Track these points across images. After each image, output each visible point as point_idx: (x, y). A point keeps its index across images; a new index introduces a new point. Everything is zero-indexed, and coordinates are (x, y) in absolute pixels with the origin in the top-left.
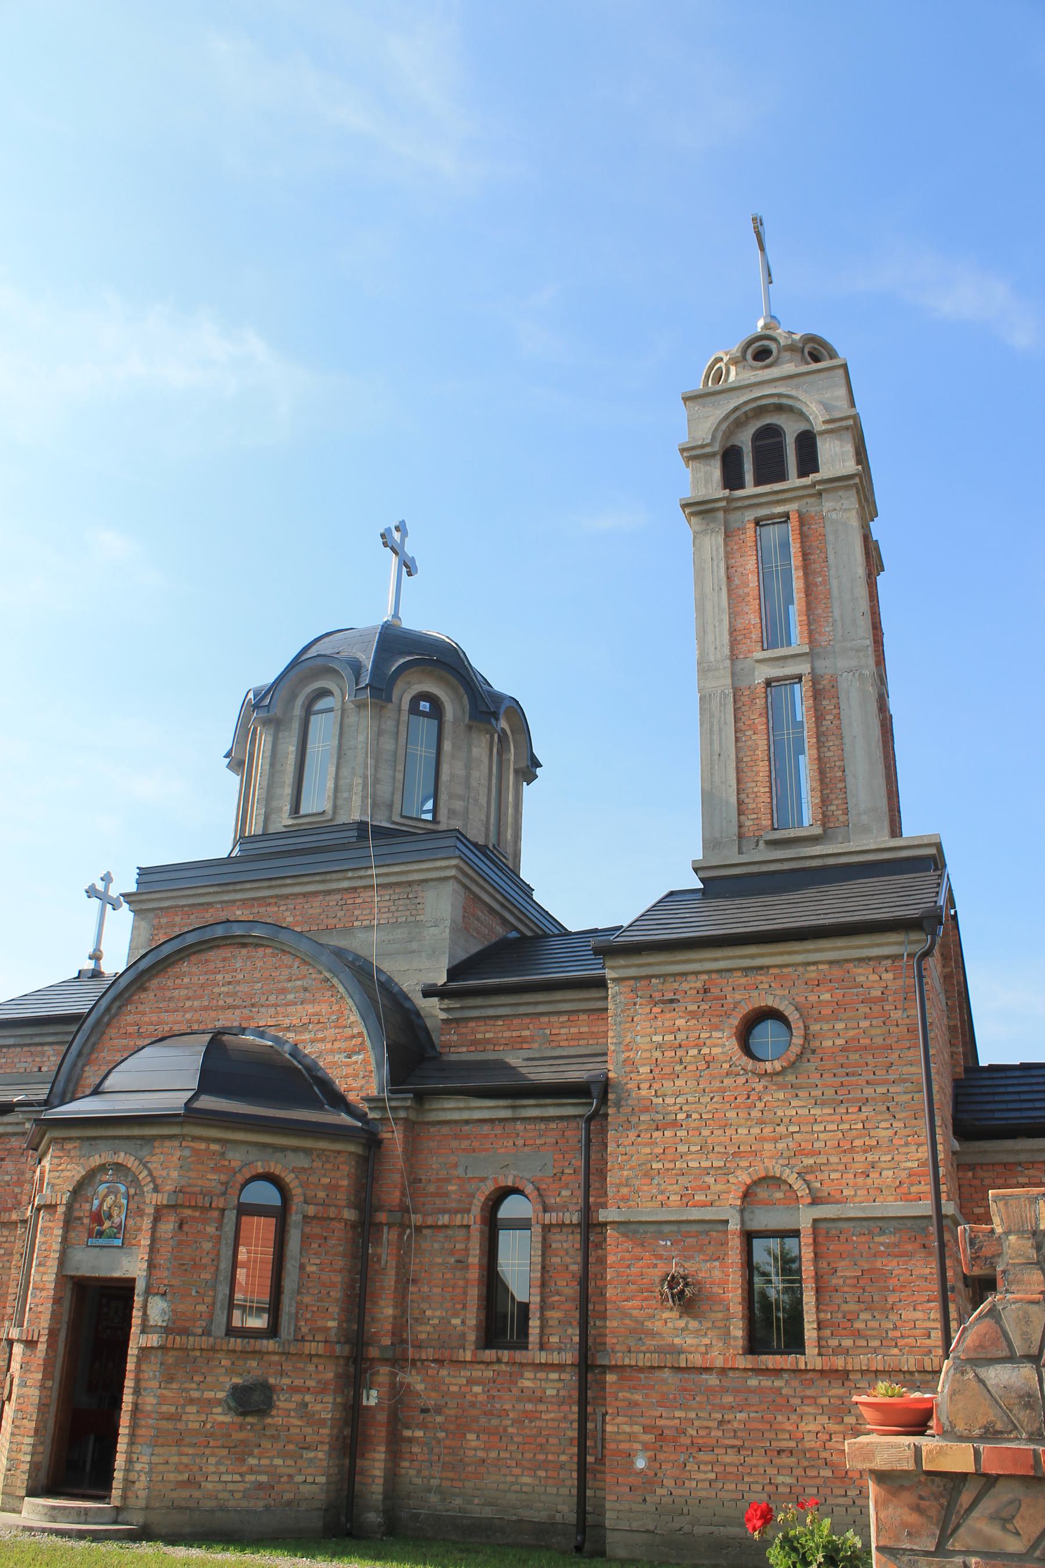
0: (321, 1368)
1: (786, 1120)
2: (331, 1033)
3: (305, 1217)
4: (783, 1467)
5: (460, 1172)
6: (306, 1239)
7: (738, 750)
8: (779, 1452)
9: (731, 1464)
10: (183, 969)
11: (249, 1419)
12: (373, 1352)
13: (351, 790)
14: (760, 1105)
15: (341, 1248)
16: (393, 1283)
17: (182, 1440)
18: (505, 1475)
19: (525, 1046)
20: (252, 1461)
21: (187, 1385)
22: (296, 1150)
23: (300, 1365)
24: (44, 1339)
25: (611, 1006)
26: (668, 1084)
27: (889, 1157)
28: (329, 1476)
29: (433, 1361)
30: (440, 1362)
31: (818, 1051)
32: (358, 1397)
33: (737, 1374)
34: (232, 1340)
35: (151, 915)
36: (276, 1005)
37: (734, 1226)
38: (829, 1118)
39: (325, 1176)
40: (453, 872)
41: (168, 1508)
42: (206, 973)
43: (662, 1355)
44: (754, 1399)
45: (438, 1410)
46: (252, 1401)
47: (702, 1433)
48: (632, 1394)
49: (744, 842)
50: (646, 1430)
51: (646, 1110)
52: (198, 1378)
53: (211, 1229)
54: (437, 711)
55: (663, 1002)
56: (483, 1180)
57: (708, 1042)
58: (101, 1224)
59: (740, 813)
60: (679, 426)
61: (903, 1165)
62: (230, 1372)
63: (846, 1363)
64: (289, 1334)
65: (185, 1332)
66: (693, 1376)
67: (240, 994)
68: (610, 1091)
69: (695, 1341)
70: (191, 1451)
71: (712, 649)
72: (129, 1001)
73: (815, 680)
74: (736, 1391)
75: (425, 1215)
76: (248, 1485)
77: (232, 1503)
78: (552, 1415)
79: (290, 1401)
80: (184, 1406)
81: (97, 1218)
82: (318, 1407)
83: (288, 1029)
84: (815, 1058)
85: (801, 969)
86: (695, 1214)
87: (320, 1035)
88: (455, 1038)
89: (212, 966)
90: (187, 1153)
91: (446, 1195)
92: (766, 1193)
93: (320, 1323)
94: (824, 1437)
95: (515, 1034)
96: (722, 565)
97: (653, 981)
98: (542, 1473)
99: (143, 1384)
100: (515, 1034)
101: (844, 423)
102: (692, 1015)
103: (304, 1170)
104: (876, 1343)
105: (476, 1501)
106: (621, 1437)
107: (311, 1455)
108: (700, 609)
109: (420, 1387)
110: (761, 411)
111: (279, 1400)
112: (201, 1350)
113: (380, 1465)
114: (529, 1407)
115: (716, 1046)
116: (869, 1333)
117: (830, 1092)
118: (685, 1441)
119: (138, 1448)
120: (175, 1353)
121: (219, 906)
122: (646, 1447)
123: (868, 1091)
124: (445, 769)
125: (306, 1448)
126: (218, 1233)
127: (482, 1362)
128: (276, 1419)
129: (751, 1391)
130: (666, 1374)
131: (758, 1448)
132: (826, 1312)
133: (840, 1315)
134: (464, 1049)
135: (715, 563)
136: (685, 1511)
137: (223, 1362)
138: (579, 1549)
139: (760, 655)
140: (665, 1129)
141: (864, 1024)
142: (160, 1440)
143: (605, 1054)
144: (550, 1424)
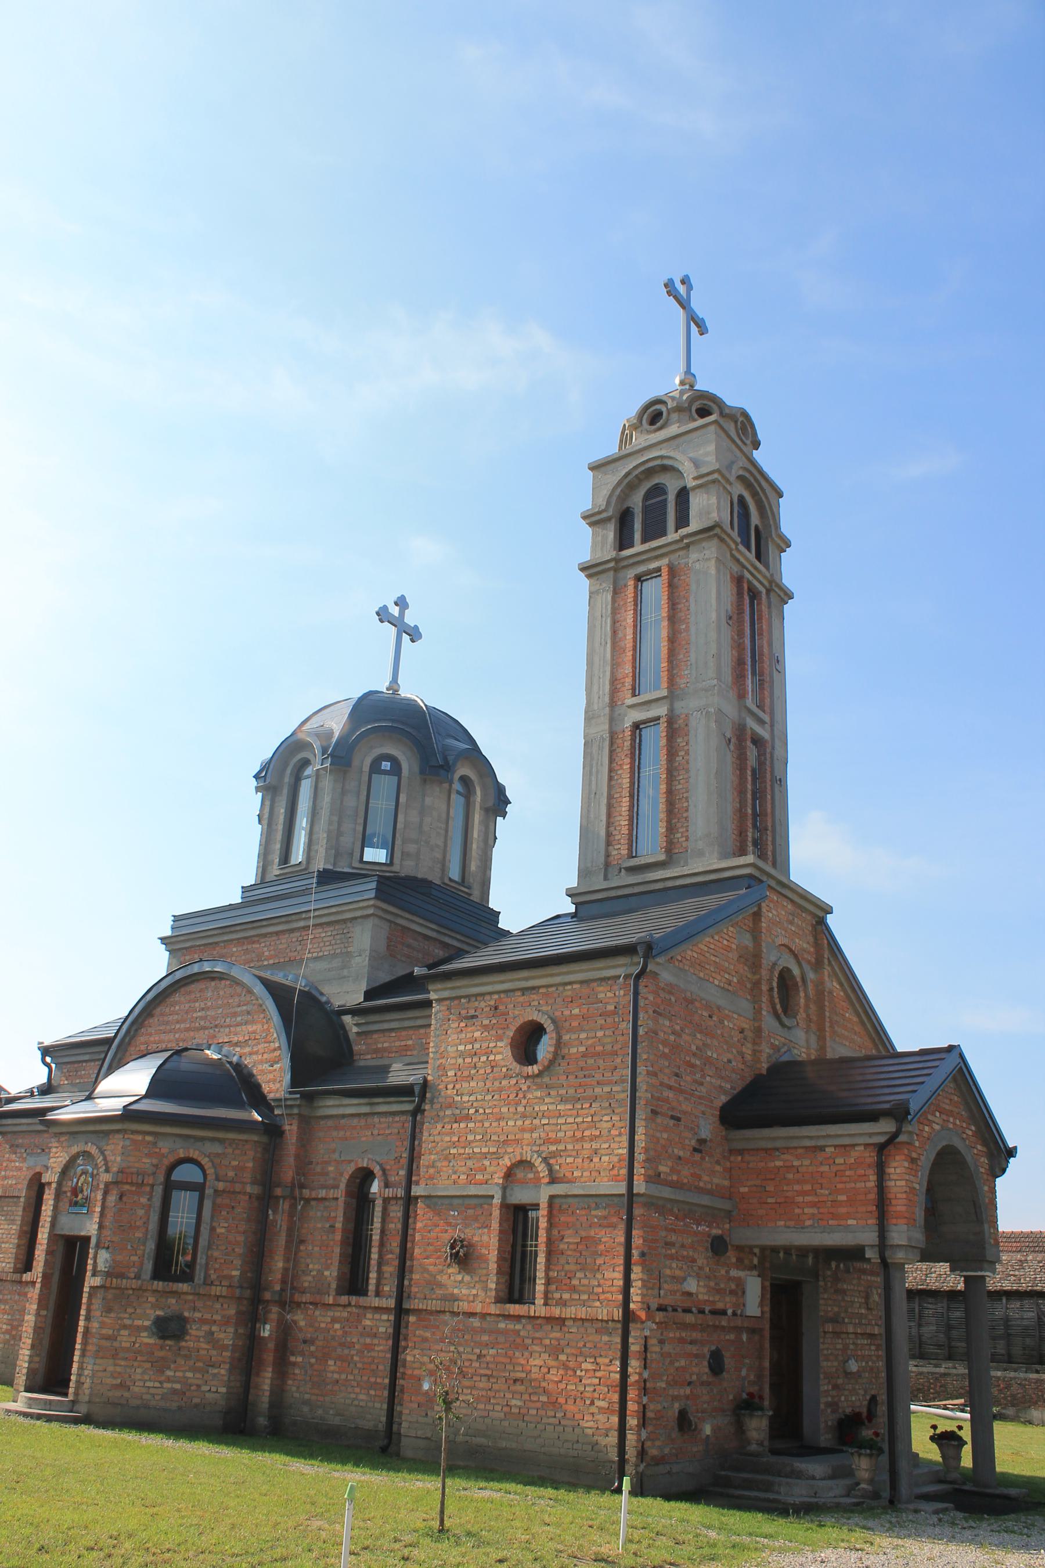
0: (225, 1306)
1: (540, 1114)
2: (261, 1047)
3: (216, 1191)
5: (336, 1156)
6: (216, 1209)
7: (610, 787)
8: (515, 1381)
11: (168, 1342)
14: (524, 1102)
19: (409, 1053)
21: (122, 1315)
22: (213, 1140)
23: (210, 1303)
24: (39, 1280)
25: (433, 1022)
26: (465, 1085)
27: (606, 1146)
28: (228, 1388)
29: (311, 1303)
32: (253, 1329)
33: (493, 1319)
35: (180, 953)
36: (229, 1026)
37: (497, 1201)
38: (569, 1113)
39: (234, 1159)
40: (371, 911)
42: (189, 1001)
44: (501, 1339)
46: (171, 1329)
47: (467, 1364)
49: (610, 869)
51: (450, 1106)
52: (130, 1310)
53: (144, 1200)
54: (396, 768)
55: (467, 1018)
56: (350, 1162)
58: (77, 1197)
59: (608, 843)
60: (583, 493)
61: (616, 1152)
62: (154, 1307)
64: (199, 1279)
65: (121, 1276)
69: (464, 1291)
70: (123, 1363)
71: (596, 700)
72: (142, 1025)
73: (671, 721)
74: (491, 1332)
75: (312, 1189)
77: (153, 1403)
78: (381, 1348)
80: (119, 1330)
82: (222, 1336)
83: (236, 1044)
84: (564, 1063)
85: (561, 988)
86: (473, 1190)
87: (255, 1049)
89: (193, 996)
90: (128, 1143)
93: (225, 1272)
94: (544, 1370)
96: (609, 621)
97: (463, 1000)
98: (372, 1392)
99: (92, 1314)
100: (403, 1043)
101: (710, 478)
102: (486, 1028)
103: (218, 1155)
104: (585, 1297)
105: (331, 1412)
106: (416, 1365)
107: (216, 1371)
108: (590, 663)
109: (302, 1323)
110: (650, 472)
112: (133, 1289)
113: (268, 1381)
114: (368, 1340)
115: (499, 1053)
116: (581, 1288)
117: (571, 1091)
119: (86, 1360)
120: (113, 1291)
123: (598, 1090)
124: (401, 818)
125: (212, 1366)
127: (339, 1305)
129: (499, 1332)
130: (447, 1317)
133: (563, 1274)
134: (369, 1057)
138: (384, 1450)
139: (630, 701)
141: (600, 1034)
142: (101, 1354)
143: (427, 1062)
144: (381, 1354)
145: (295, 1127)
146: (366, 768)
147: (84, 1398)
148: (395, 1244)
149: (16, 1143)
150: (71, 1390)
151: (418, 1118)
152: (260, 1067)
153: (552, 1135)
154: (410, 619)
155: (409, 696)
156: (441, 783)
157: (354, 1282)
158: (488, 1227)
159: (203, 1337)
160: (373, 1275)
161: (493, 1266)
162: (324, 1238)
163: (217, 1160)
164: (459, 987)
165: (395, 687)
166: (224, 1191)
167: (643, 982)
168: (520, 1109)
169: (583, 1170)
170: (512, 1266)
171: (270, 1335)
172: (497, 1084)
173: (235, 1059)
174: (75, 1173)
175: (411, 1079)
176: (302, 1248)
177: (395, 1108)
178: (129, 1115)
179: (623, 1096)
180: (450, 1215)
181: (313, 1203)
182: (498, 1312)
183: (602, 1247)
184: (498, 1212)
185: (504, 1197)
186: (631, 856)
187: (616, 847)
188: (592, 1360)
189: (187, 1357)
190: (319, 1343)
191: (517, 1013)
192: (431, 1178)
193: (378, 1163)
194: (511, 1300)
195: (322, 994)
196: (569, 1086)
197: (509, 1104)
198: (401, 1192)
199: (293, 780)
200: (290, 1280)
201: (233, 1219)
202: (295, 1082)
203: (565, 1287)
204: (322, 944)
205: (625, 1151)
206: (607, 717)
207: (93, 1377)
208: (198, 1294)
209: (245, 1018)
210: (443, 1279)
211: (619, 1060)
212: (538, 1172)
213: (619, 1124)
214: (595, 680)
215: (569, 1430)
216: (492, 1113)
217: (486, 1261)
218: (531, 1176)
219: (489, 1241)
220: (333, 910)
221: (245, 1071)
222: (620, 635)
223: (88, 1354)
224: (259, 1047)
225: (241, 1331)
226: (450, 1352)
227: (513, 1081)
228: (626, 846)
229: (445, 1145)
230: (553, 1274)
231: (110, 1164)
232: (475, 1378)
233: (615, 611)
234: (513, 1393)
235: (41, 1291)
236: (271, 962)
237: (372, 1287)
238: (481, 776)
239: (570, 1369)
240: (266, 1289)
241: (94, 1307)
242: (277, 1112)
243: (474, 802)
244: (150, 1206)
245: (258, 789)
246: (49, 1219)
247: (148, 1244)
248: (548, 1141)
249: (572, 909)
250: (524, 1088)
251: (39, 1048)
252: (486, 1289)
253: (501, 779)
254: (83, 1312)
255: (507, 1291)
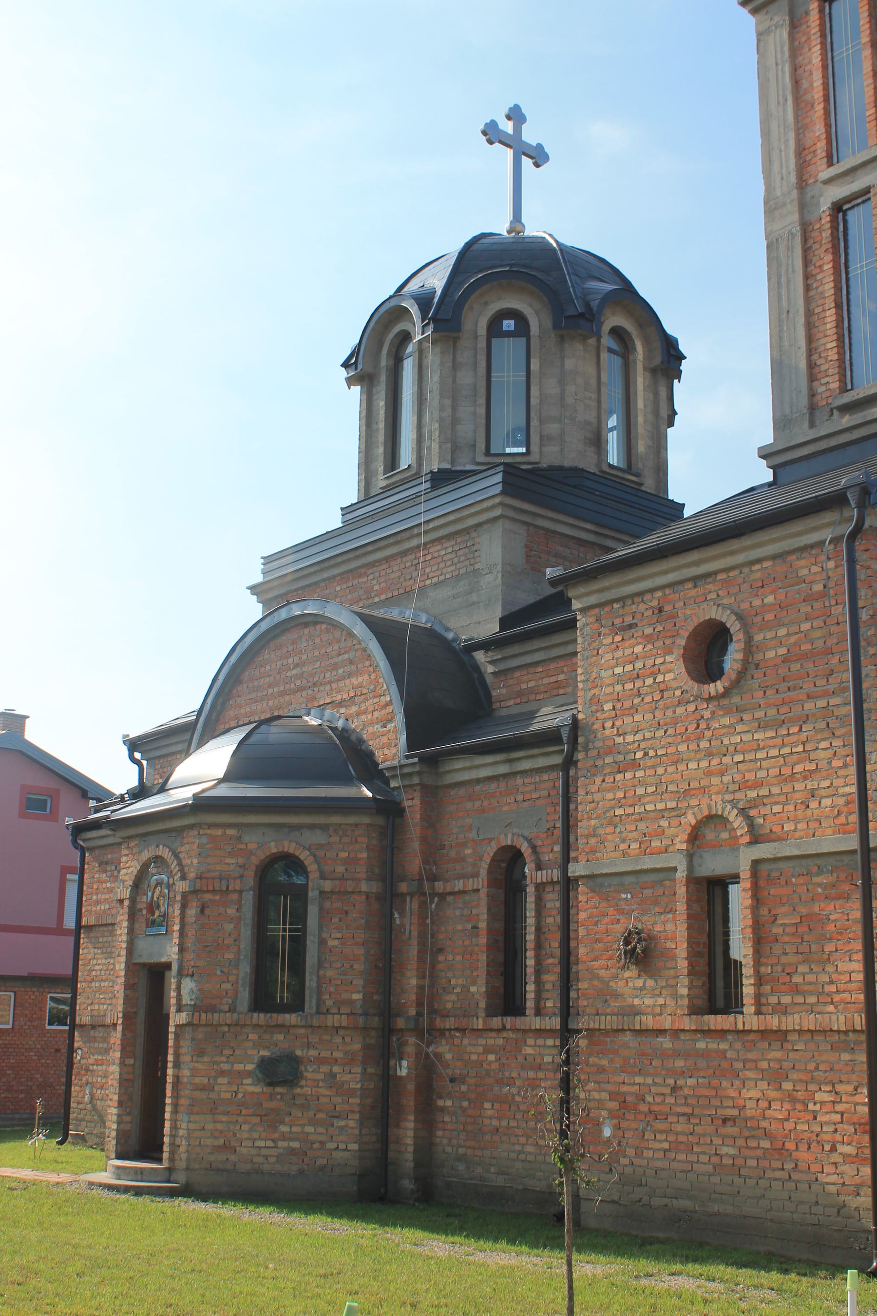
0: (348, 1039)
4: (727, 1136)
5: (473, 835)
7: (808, 300)
8: (724, 1121)
9: (682, 1133)
10: (266, 657)
11: (279, 1090)
12: (400, 1023)
13: (430, 438)
14: (708, 734)
15: (363, 921)
16: (416, 953)
17: (216, 1108)
18: (514, 1144)
19: (561, 691)
20: (284, 1129)
22: (312, 827)
24: (120, 1022)
26: (628, 720)
27: (826, 784)
29: (457, 1029)
30: (463, 1031)
31: (762, 665)
32: (386, 1067)
33: (688, 1036)
34: (255, 1015)
38: (771, 742)
39: (343, 850)
40: (498, 512)
41: (206, 1169)
43: (620, 1017)
44: (702, 1063)
45: (462, 1080)
46: (280, 1072)
47: (658, 1099)
48: (600, 1059)
50: (613, 1096)
51: (609, 752)
52: (227, 1052)
53: (231, 911)
54: (523, 328)
57: (662, 668)
58: (153, 915)
61: (841, 791)
63: (780, 1022)
64: (311, 1008)
65: (212, 1009)
66: (649, 1039)
67: (305, 675)
68: (579, 734)
69: (648, 1001)
70: (224, 1118)
71: (778, 184)
74: (686, 1056)
76: (281, 1151)
77: (266, 1167)
79: (319, 1072)
80: (215, 1078)
81: (152, 907)
82: (347, 1077)
83: (341, 704)
84: (758, 674)
85: (746, 570)
86: (648, 863)
87: (363, 707)
88: (504, 691)
89: (285, 650)
90: (204, 840)
91: (463, 859)
92: (713, 834)
93: (345, 996)
94: (763, 1104)
95: (552, 679)
96: (787, 68)
97: (615, 606)
99: (182, 1058)
100: (552, 679)
102: (649, 639)
103: (321, 846)
104: (812, 999)
105: (493, 1170)
107: (342, 1123)
108: (766, 134)
109: (448, 1056)
111: (307, 1071)
112: (229, 1025)
113: (410, 1133)
114: (531, 1074)
115: (669, 671)
116: (807, 987)
117: (772, 712)
118: (644, 1108)
119: (180, 1116)
121: (323, 584)
122: (612, 1115)
123: (809, 706)
126: (238, 914)
127: (492, 1030)
128: (305, 1089)
130: (628, 1037)
131: (705, 1115)
132: (765, 964)
133: (779, 969)
134: (511, 702)
135: (780, 67)
136: (644, 1182)
137: (251, 1036)
139: (825, 174)
140: (626, 771)
141: (805, 626)
145: (417, 802)
146: (482, 331)
147: (181, 1164)
148: (554, 944)
149: (105, 859)
150: (165, 1155)
151: (572, 773)
152: (370, 730)
153: (750, 776)
154: (530, 135)
155: (535, 234)
156: (585, 338)
157: (508, 1000)
158: (672, 911)
159: (322, 1080)
160: (531, 987)
161: (683, 964)
162: (467, 943)
163: (320, 853)
164: (608, 588)
165: (519, 228)
166: (332, 892)
167: (860, 545)
168: (704, 744)
169: (796, 821)
170: (711, 963)
171: (408, 1074)
172: (669, 713)
173: (340, 724)
174: (149, 886)
175: (556, 723)
176: (441, 958)
177: (542, 762)
178: (202, 805)
179: (844, 710)
180: (621, 899)
181: (450, 898)
182: (694, 1028)
183: (831, 927)
184: (684, 889)
185: (690, 868)
186: (844, 390)
187: (823, 381)
188: (829, 1088)
189: (304, 1107)
190: (471, 1081)
191: (689, 612)
192: (593, 851)
193: (525, 838)
194: (713, 1010)
195: (448, 629)
196: (769, 706)
197: (688, 739)
198: (556, 874)
199: (392, 362)
200: (429, 1001)
201: (348, 927)
202: (412, 744)
203: (783, 987)
204: (442, 565)
205: (853, 789)
206: (796, 203)
207: (188, 1138)
208: (311, 1026)
209: (348, 669)
210: (618, 986)
211: (835, 660)
212: (734, 830)
213: (842, 752)
214: (775, 155)
215: (804, 1186)
216: (666, 755)
217: (674, 957)
218: (725, 835)
219: (674, 930)
220: (452, 518)
221: (353, 738)
222: (805, 84)
223: (181, 1109)
224: (368, 703)
225: (371, 1070)
226: (634, 1084)
227: (691, 707)
228: (837, 377)
229: (608, 805)
230: (765, 970)
231: (186, 869)
232: (670, 1119)
233: (794, 52)
234: (724, 1137)
235: (123, 1034)
236: (383, 597)
237: (530, 1004)
238: (641, 326)
239: (799, 1101)
240: (399, 1015)
241: (183, 1050)
242: (393, 784)
243: (635, 361)
244: (240, 918)
245: (350, 382)
246: (124, 945)
247: (241, 967)
248: (744, 785)
249: (768, 476)
250: (707, 714)
251: (124, 742)
252: (675, 996)
253: (670, 329)
254: (170, 1058)
255: (706, 997)
